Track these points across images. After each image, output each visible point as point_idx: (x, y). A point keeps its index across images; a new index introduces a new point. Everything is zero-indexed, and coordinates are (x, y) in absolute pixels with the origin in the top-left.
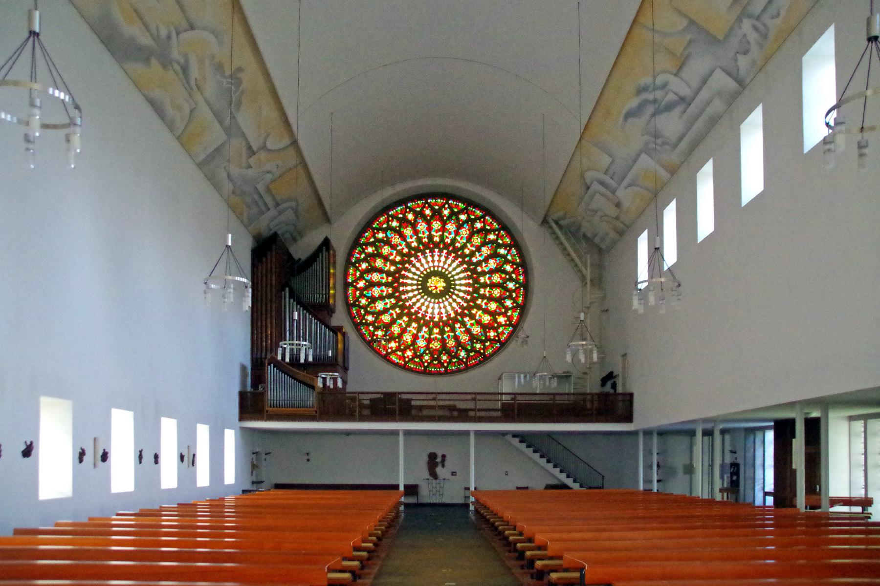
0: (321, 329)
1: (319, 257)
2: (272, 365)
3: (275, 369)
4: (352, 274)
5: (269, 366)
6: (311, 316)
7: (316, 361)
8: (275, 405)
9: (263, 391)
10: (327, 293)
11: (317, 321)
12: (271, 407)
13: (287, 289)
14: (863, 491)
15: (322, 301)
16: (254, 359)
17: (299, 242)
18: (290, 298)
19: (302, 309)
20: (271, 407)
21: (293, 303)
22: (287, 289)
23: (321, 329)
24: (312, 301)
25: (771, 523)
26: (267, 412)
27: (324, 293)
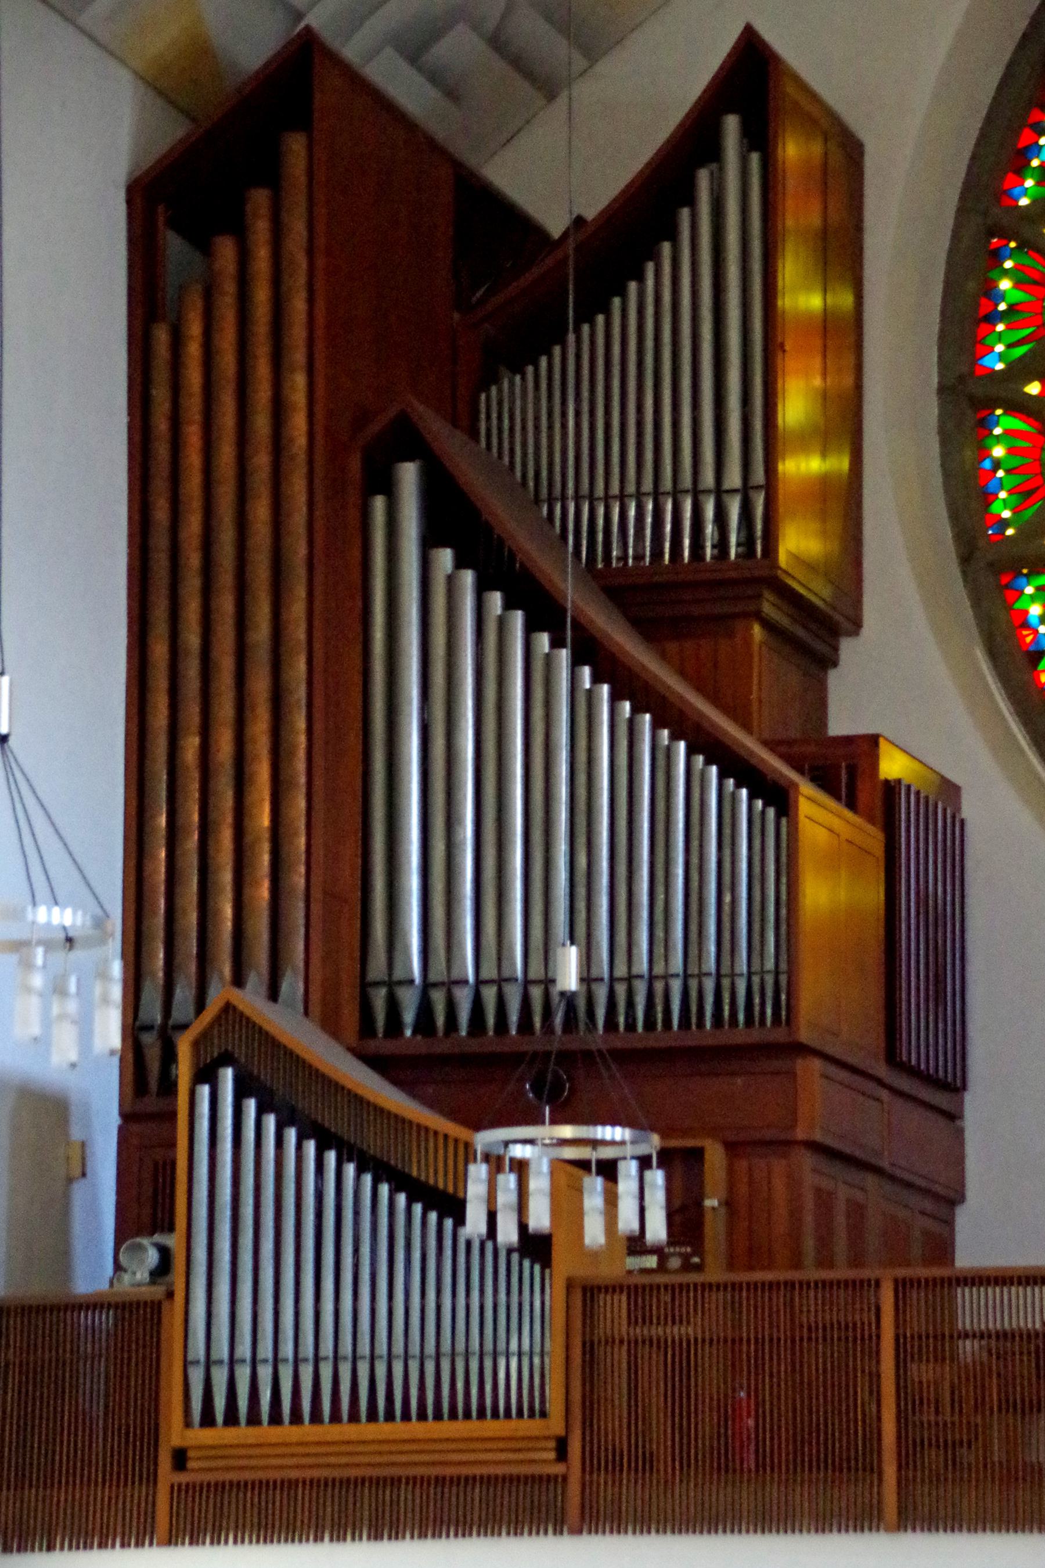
0: (662, 761)
1: (691, 202)
2: (228, 1075)
3: (251, 1106)
4: (1013, 308)
5: (205, 1090)
6: (586, 671)
7: (631, 1026)
8: (344, 1486)
9: (158, 1292)
10: (759, 476)
11: (635, 710)
12: (208, 1419)
13: (409, 474)
14: (495, 972)
15: (639, 557)
16: (149, 1039)
17: (585, 91)
18: (429, 542)
19: (518, 618)
20: (208, 1419)
21: (451, 580)
22: (409, 474)
23: (662, 761)
24: (722, 545)
25: (551, 1112)
26: (180, 1458)
27: (734, 478)
